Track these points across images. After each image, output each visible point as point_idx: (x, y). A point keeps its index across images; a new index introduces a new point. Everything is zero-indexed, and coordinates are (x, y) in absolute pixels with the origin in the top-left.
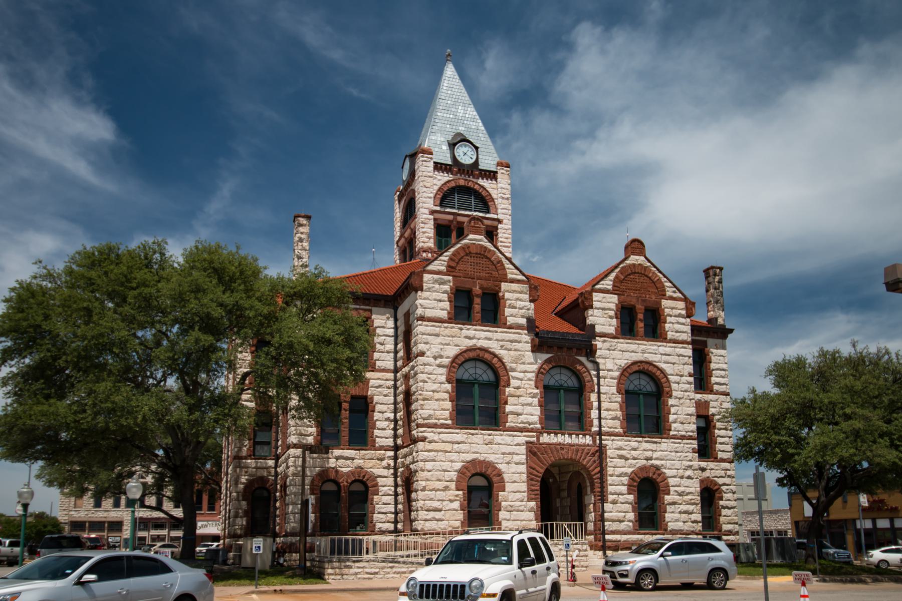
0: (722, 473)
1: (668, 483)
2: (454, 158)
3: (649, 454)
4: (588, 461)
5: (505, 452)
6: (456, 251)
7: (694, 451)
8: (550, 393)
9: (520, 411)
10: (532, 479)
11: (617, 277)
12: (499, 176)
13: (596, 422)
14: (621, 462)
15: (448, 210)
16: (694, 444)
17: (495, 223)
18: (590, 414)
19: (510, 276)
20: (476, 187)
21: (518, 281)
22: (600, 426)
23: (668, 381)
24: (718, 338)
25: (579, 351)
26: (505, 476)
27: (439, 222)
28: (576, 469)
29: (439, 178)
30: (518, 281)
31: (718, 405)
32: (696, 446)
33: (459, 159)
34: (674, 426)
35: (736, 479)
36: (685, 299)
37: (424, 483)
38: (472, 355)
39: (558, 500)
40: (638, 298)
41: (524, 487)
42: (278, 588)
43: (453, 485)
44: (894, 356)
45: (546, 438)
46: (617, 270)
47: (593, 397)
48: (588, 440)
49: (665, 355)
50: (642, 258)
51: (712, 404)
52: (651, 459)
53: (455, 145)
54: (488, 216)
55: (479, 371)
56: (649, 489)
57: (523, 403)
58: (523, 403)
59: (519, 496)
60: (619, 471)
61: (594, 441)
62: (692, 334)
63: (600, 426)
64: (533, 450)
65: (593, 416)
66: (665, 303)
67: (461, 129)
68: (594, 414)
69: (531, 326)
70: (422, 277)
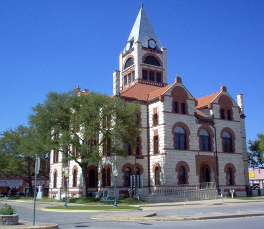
8: (202, 138)
13: (215, 148)
15: (147, 64)
17: (162, 70)
21: (192, 100)
22: (216, 150)
30: (192, 100)
36: (195, 100)
43: (175, 170)
47: (214, 139)
48: (212, 154)
54: (159, 67)
55: (180, 130)
57: (194, 142)
58: (194, 142)
63: (216, 150)
64: (198, 158)
68: (214, 145)
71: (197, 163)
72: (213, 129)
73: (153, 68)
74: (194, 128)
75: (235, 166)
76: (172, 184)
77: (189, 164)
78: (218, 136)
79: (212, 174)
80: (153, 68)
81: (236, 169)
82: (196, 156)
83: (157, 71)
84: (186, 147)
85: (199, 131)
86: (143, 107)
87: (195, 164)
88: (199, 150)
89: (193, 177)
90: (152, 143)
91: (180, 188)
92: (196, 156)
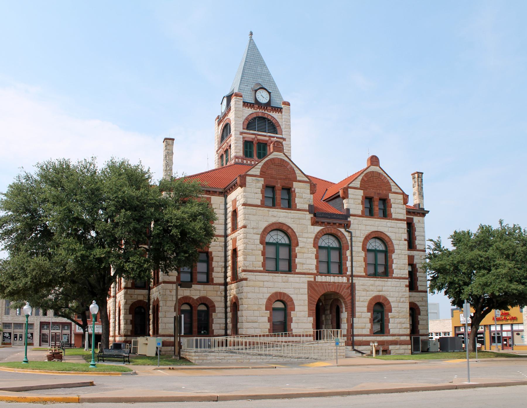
0: (421, 299)
1: (391, 305)
2: (256, 99)
3: (380, 288)
4: (345, 293)
5: (296, 288)
6: (266, 162)
7: (406, 286)
9: (304, 262)
10: (311, 303)
11: (363, 179)
12: (283, 110)
13: (349, 269)
14: (364, 293)
16: (407, 282)
18: (346, 264)
19: (298, 178)
20: (269, 118)
23: (392, 243)
24: (420, 216)
25: (340, 225)
26: (295, 302)
27: (246, 139)
28: (336, 297)
29: (246, 111)
31: (419, 259)
32: (408, 284)
33: (259, 100)
34: (395, 271)
35: (439, 302)
36: (403, 193)
37: (246, 306)
38: (285, 228)
39: (324, 316)
40: (375, 193)
41: (306, 308)
42: (171, 367)
43: (264, 307)
44: (522, 231)
45: (319, 279)
46: (363, 175)
47: (348, 253)
48: (344, 280)
49: (391, 227)
50: (378, 167)
51: (415, 257)
52: (382, 291)
53: (256, 91)
56: (380, 309)
57: (306, 258)
58: (306, 258)
59: (303, 313)
60: (361, 300)
61: (348, 280)
62: (407, 214)
65: (347, 266)
66: (391, 196)
67: (260, 81)
68: (349, 264)
69: (312, 209)
70: (245, 178)
71: (310, 296)
72: (346, 234)
73: (264, 136)
74: (306, 231)
75: (390, 299)
76: (258, 332)
77: (293, 297)
78: (358, 247)
79: (344, 315)
80: (264, 136)
81: (393, 305)
82: (309, 283)
83: (258, 140)
84: (387, 273)
85: (317, 238)
86: (216, 201)
87: (306, 297)
88: (315, 272)
89: (302, 320)
90: (229, 258)
91: (273, 339)
92: (309, 283)
